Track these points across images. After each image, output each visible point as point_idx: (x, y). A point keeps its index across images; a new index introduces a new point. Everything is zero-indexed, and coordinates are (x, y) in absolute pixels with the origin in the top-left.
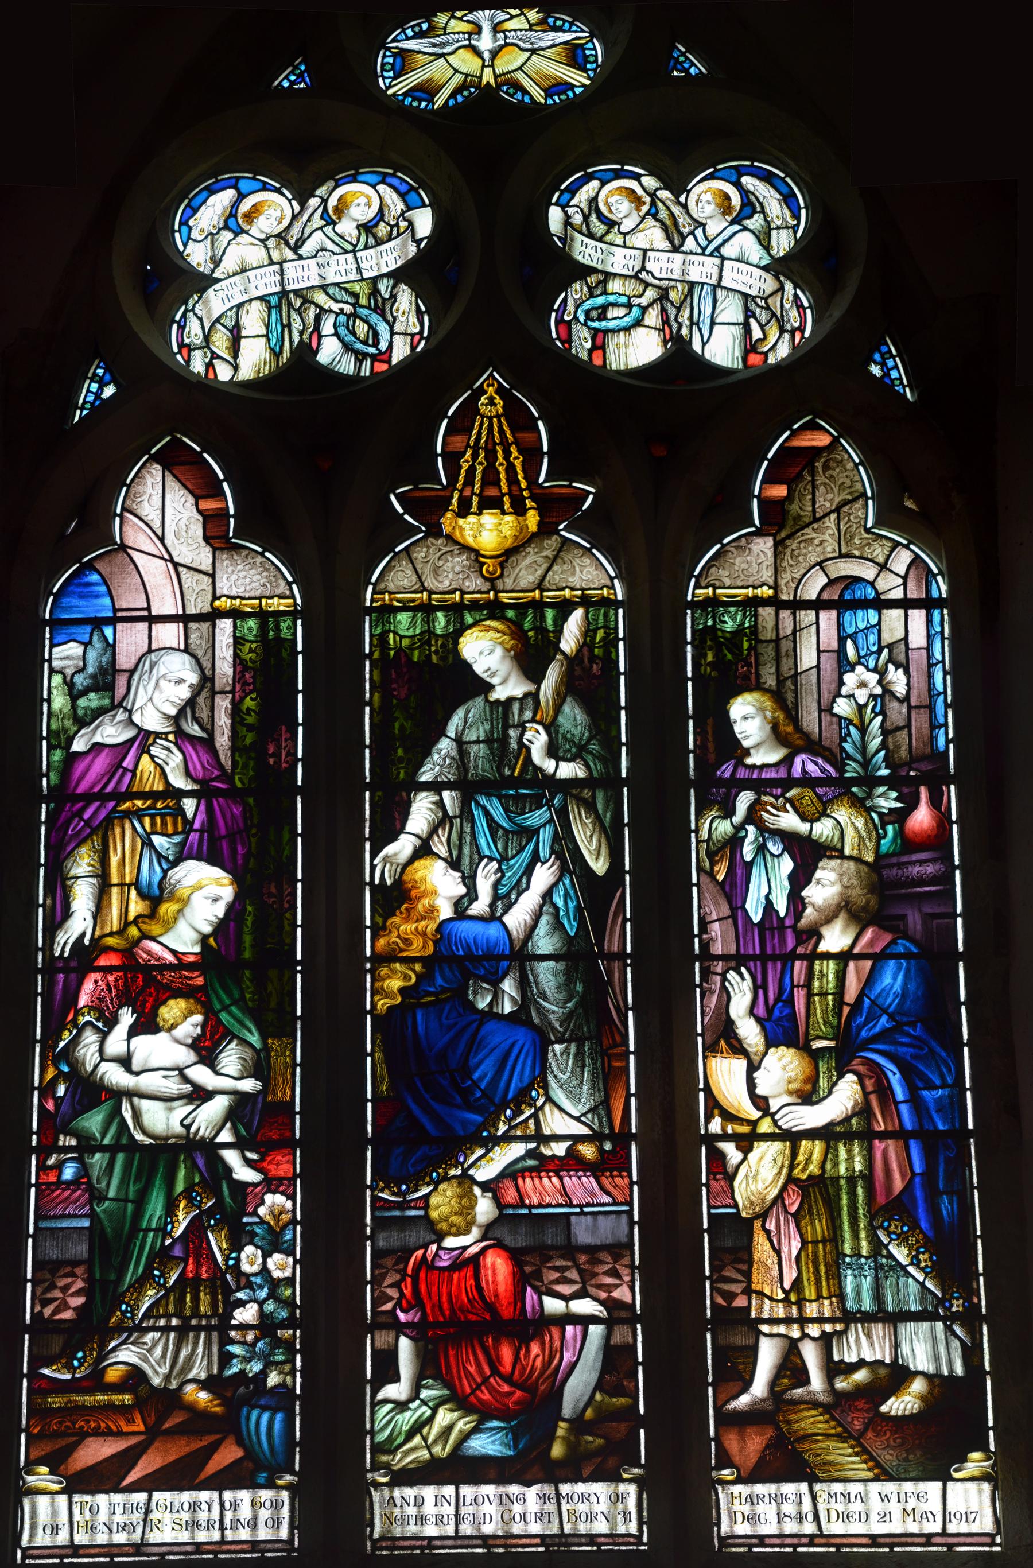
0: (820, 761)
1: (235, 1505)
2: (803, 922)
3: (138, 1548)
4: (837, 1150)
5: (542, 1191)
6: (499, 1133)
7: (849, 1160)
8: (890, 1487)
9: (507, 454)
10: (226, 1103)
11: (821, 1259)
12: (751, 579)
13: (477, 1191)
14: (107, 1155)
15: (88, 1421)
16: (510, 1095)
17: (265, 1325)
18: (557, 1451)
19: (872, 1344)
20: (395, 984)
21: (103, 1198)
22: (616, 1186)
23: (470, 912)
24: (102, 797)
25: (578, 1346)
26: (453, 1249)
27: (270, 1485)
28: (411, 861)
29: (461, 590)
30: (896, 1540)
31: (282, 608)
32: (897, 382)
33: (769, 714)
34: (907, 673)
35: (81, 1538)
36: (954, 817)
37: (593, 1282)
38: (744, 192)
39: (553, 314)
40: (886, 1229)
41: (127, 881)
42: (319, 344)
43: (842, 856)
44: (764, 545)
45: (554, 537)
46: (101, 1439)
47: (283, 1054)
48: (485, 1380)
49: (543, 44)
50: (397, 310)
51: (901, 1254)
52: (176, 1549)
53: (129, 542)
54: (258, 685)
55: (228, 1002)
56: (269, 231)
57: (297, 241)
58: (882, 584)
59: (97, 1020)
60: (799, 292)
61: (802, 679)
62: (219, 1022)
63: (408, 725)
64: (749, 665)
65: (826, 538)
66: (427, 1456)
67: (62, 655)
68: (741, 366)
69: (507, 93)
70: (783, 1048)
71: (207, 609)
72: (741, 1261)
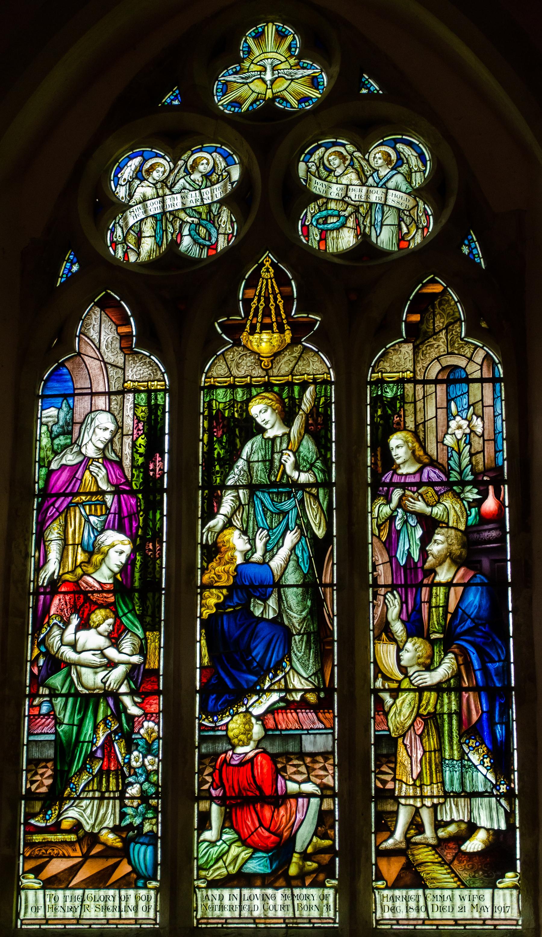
0: (437, 471)
1: (127, 898)
2: (427, 565)
3: (78, 920)
4: (442, 697)
5: (288, 721)
6: (265, 688)
7: (449, 703)
8: (466, 892)
9: (275, 299)
10: (125, 670)
11: (433, 761)
12: (401, 367)
13: (253, 720)
14: (64, 699)
15: (53, 850)
16: (272, 666)
17: (144, 797)
18: (293, 870)
19: (458, 811)
20: (212, 601)
21: (61, 723)
22: (326, 718)
23: (252, 560)
24: (66, 495)
25: (305, 810)
26: (240, 754)
27: (145, 887)
28: (222, 530)
29: (250, 376)
30: (468, 922)
31: (159, 387)
32: (477, 256)
33: (410, 444)
34: (483, 419)
35: (50, 915)
36: (507, 504)
37: (313, 774)
38: (398, 153)
39: (300, 222)
40: (468, 744)
41: (77, 542)
42: (181, 241)
43: (448, 527)
44: (407, 349)
45: (299, 346)
46: (60, 859)
47: (154, 641)
48: (256, 829)
49: (297, 76)
50: (221, 221)
51: (475, 758)
52: (97, 922)
53: (83, 351)
54: (145, 430)
55: (126, 611)
56: (157, 179)
57: (172, 184)
58: (469, 370)
59: (60, 622)
60: (426, 207)
61: (428, 424)
62: (122, 623)
63: (222, 452)
64: (400, 416)
65: (440, 344)
66: (226, 872)
67: (47, 415)
68: (396, 249)
69: (279, 103)
70: (415, 638)
71: (121, 388)
72: (391, 762)
